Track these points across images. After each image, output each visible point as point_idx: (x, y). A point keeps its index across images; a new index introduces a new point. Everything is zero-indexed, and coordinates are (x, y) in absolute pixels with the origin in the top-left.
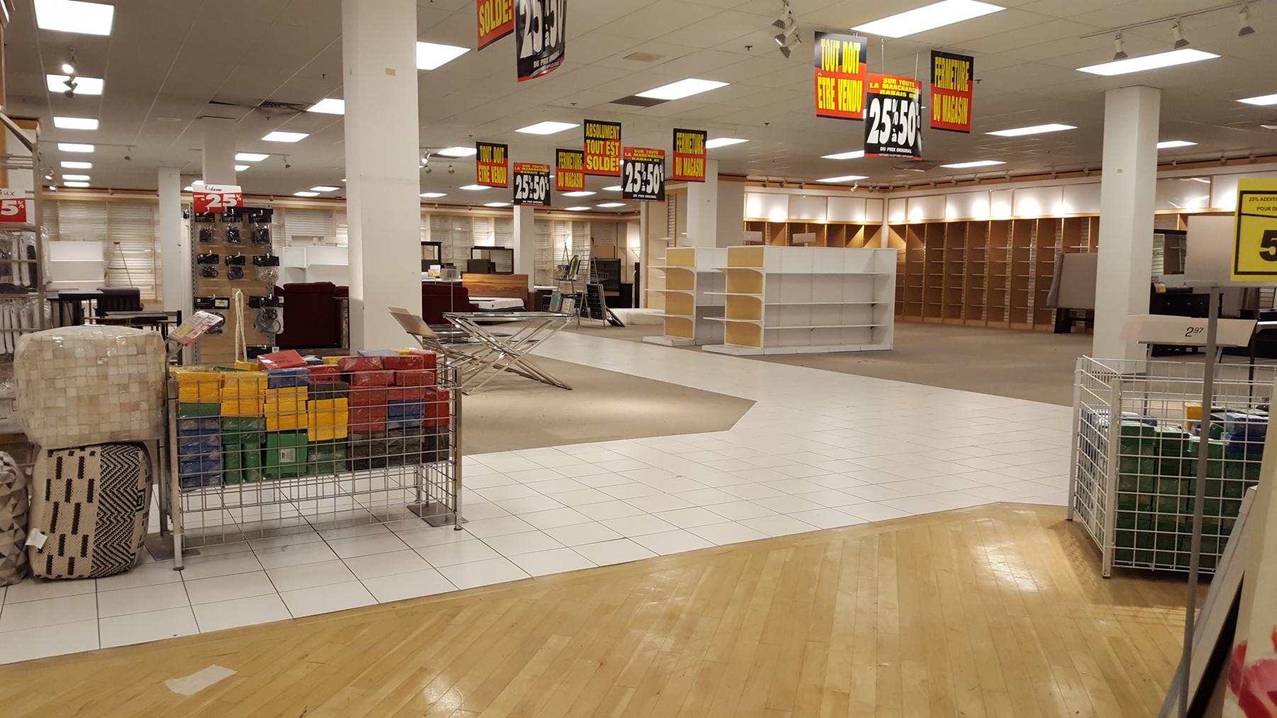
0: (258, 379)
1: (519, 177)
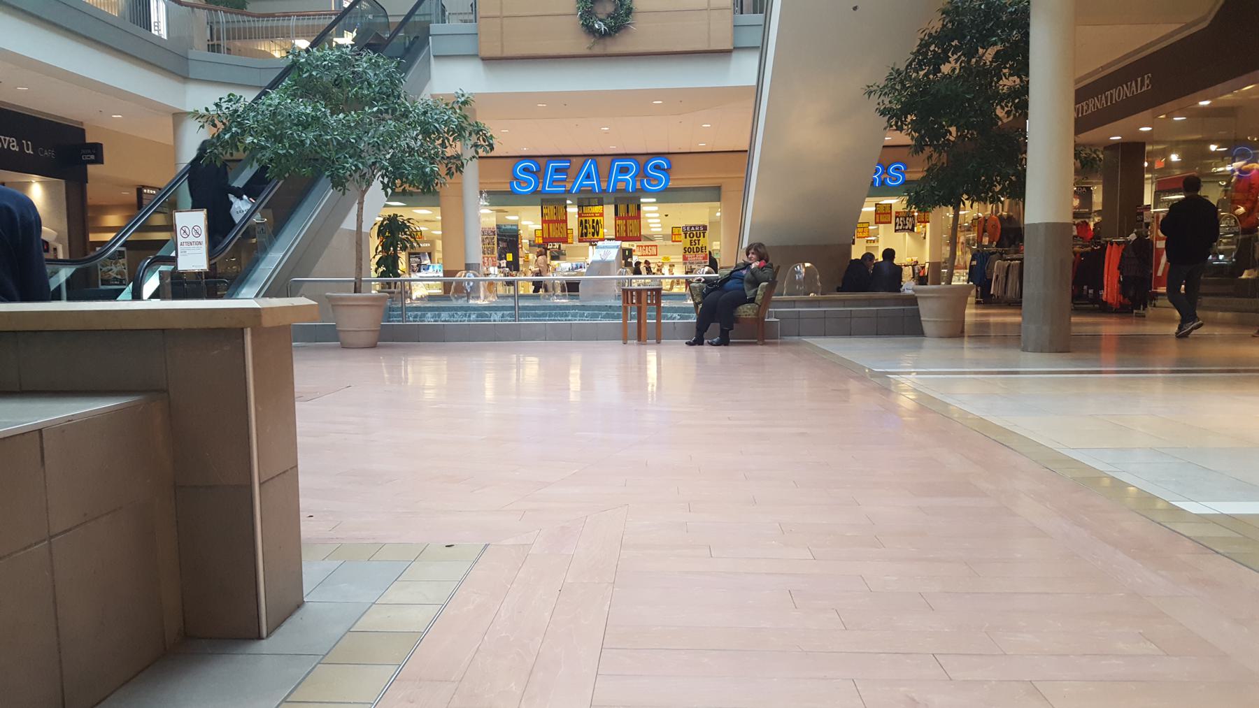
0: (140, 191)
1: (898, 219)
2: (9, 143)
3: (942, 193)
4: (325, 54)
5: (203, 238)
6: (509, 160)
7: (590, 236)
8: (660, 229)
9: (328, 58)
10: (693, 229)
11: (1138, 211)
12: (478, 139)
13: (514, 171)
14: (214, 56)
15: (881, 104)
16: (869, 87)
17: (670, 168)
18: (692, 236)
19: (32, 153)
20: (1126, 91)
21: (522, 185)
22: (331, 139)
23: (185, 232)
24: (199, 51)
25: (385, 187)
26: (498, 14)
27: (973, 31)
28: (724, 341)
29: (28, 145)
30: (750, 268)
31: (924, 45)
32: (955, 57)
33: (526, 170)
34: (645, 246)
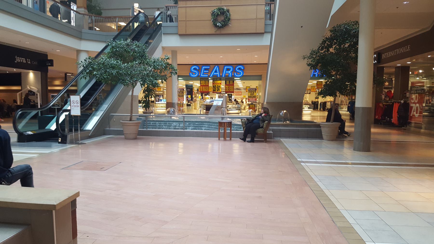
0: (66, 74)
2: (23, 60)
3: (329, 92)
4: (121, 43)
5: (79, 105)
6: (189, 65)
7: (216, 91)
8: (242, 87)
9: (122, 44)
10: (252, 90)
11: (405, 93)
12: (172, 70)
13: (191, 69)
14: (90, 31)
15: (308, 62)
16: (304, 56)
17: (244, 69)
18: (251, 92)
19: (30, 63)
20: (402, 50)
21: (193, 74)
22: (122, 72)
23: (73, 102)
24: (86, 30)
25: (141, 85)
26: (185, 19)
27: (340, 38)
28: (252, 141)
29: (29, 60)
30: (262, 116)
31: (324, 42)
32: (335, 46)
33: (195, 69)
34: (237, 92)
